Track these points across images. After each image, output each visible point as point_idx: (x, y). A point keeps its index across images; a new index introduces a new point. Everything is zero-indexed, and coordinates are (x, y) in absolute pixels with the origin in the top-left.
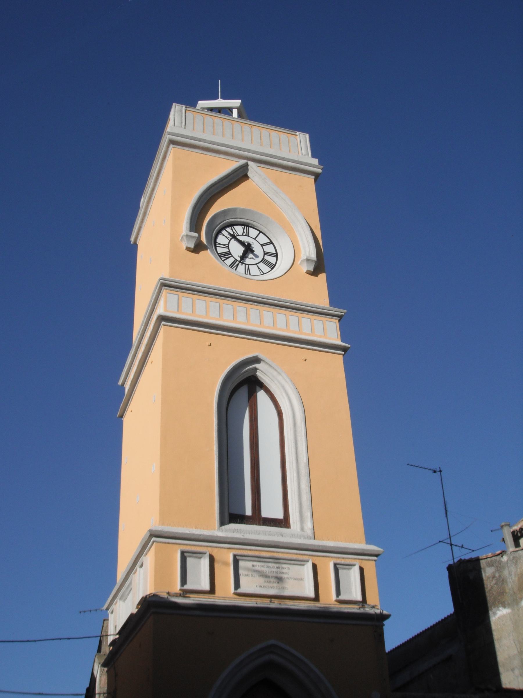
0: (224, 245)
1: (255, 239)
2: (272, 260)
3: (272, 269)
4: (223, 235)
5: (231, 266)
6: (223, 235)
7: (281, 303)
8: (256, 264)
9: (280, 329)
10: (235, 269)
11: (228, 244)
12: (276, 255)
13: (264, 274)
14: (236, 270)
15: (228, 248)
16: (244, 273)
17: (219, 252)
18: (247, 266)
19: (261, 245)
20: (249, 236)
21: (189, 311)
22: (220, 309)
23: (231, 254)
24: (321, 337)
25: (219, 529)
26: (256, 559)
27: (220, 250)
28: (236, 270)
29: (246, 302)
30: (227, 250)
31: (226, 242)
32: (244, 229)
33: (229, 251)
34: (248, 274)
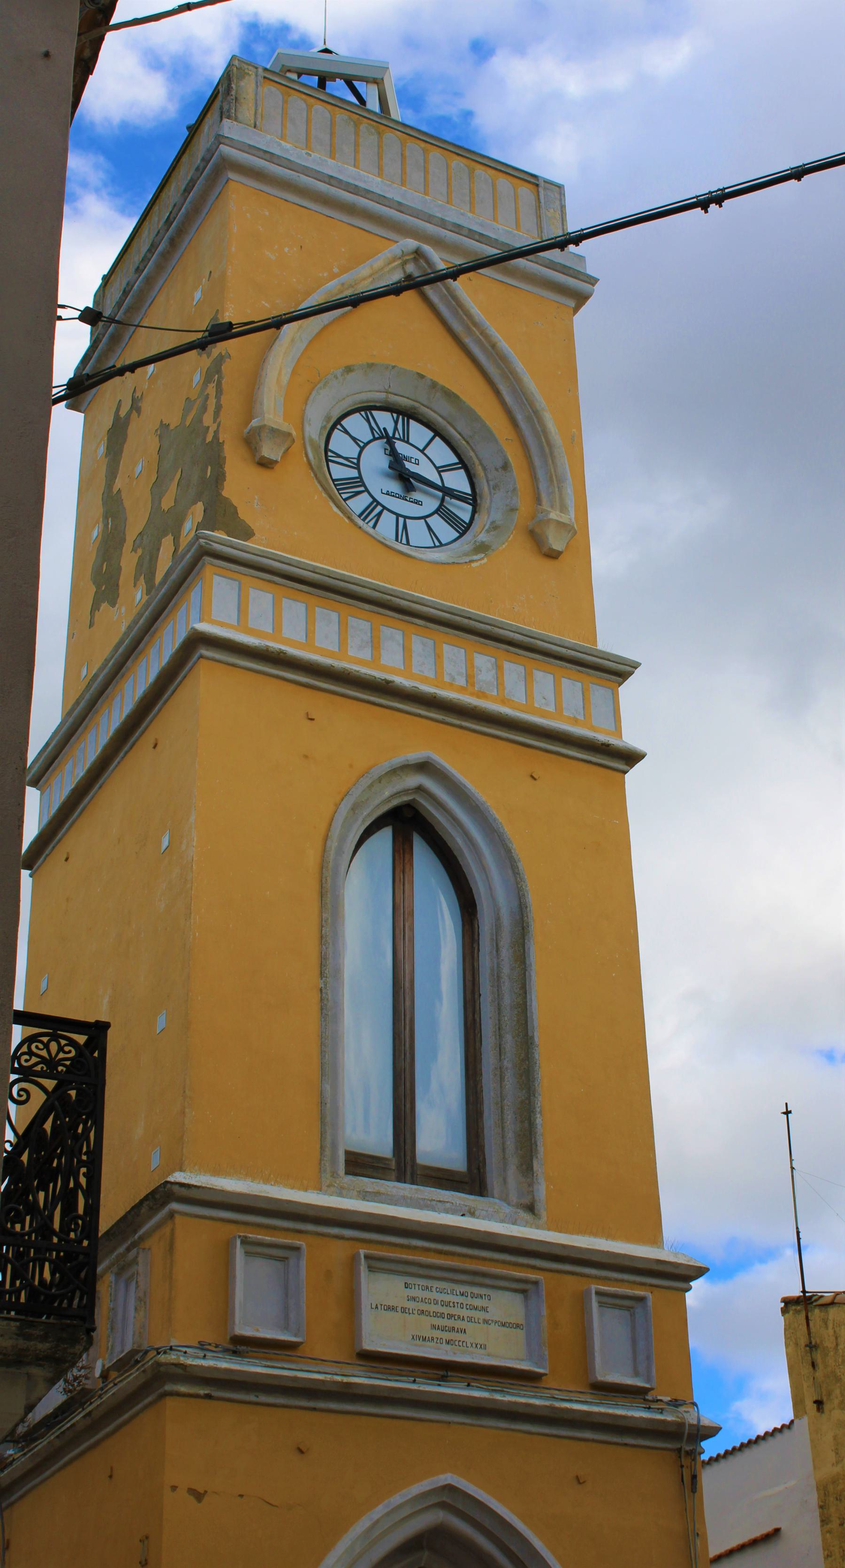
0: (347, 459)
1: (422, 451)
2: (463, 512)
3: (461, 535)
4: (346, 432)
5: (364, 514)
6: (346, 432)
7: (546, 645)
8: (424, 518)
9: (222, 624)
10: (372, 523)
11: (359, 458)
12: (473, 500)
13: (441, 545)
14: (374, 527)
15: (357, 467)
16: (394, 537)
17: (334, 478)
18: (401, 520)
19: (437, 468)
20: (408, 442)
21: (301, 637)
22: (310, 621)
23: (364, 485)
24: (575, 721)
25: (540, 1219)
26: (422, 1271)
27: (339, 472)
28: (374, 527)
29: (482, 640)
30: (354, 473)
31: (351, 450)
32: (396, 423)
33: (360, 477)
34: (404, 541)
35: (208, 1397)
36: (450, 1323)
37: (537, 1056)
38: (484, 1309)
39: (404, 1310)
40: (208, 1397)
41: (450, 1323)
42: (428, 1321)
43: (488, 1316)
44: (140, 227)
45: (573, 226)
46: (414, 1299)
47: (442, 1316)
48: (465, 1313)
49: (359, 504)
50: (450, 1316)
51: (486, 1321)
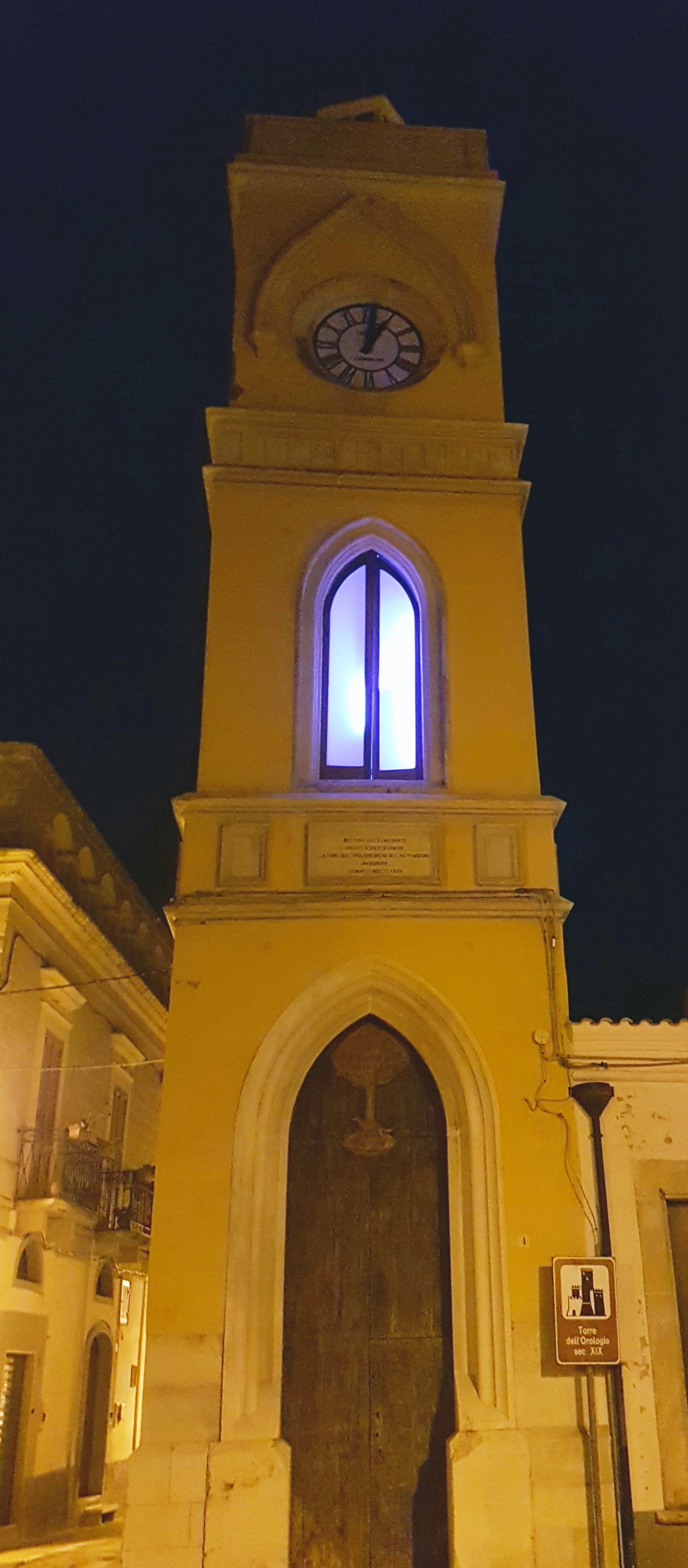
15: (338, 348)
30: (335, 351)
35: (518, 897)
36: (376, 860)
37: (683, 1374)
38: (401, 848)
39: (343, 856)
40: (518, 897)
41: (376, 860)
42: (360, 860)
43: (402, 852)
44: (442, 721)
45: (528, 887)
46: (350, 848)
47: (370, 855)
48: (387, 852)
49: (337, 371)
50: (376, 856)
51: (402, 856)
